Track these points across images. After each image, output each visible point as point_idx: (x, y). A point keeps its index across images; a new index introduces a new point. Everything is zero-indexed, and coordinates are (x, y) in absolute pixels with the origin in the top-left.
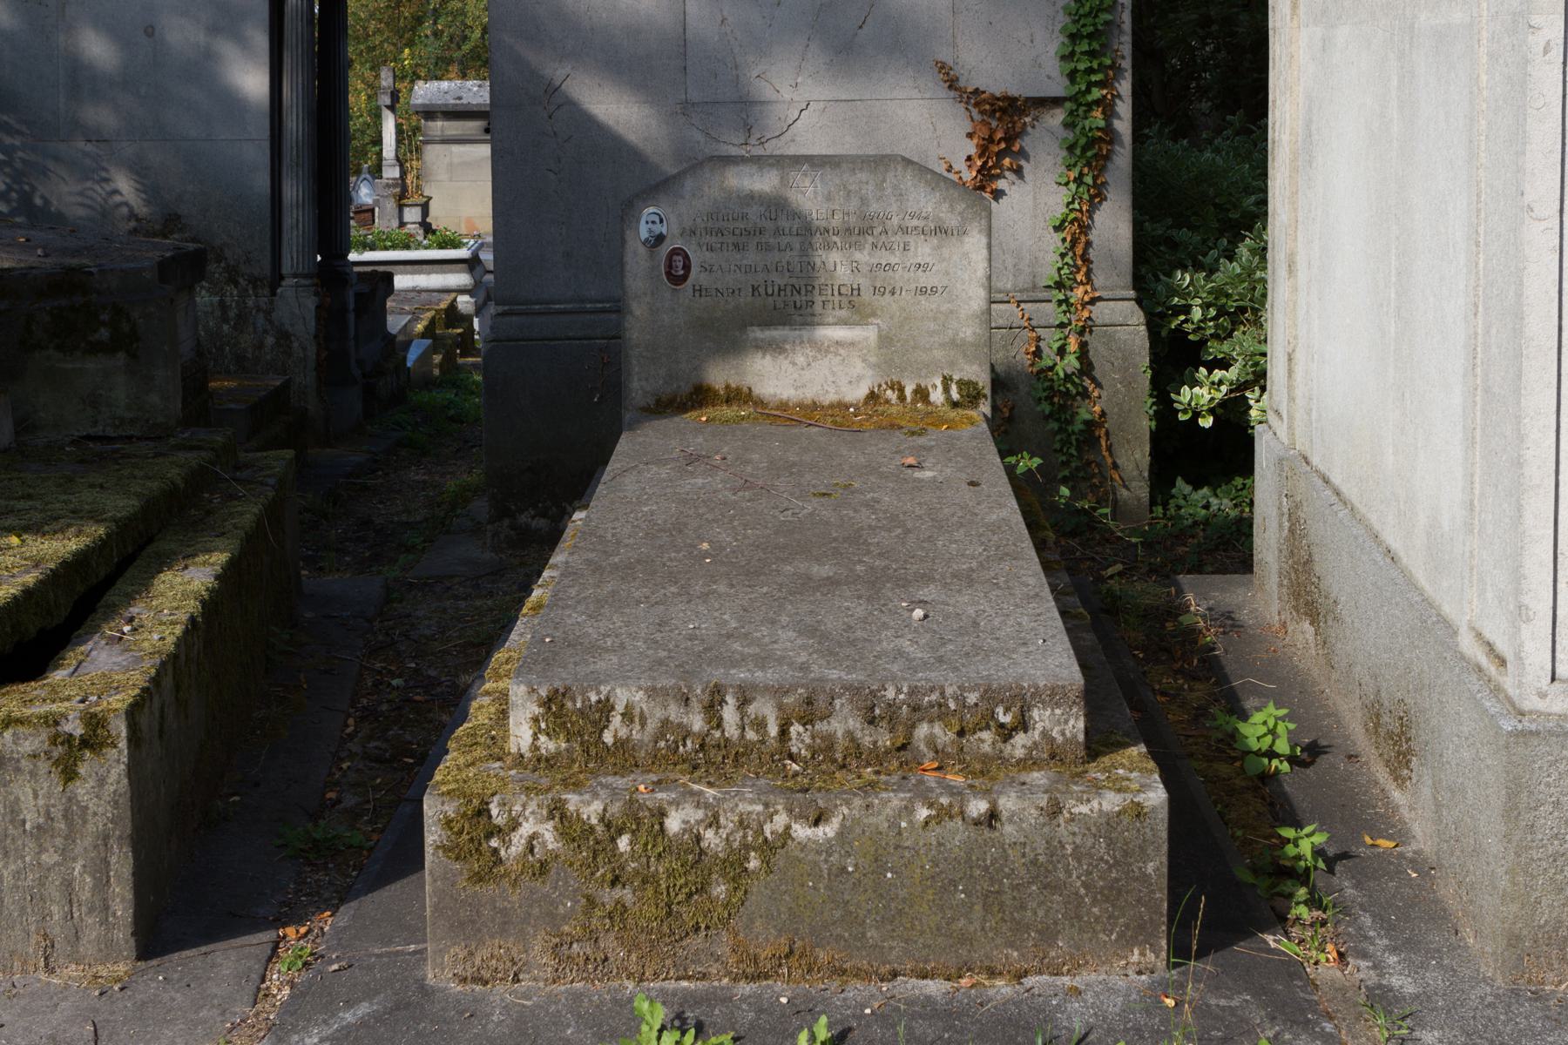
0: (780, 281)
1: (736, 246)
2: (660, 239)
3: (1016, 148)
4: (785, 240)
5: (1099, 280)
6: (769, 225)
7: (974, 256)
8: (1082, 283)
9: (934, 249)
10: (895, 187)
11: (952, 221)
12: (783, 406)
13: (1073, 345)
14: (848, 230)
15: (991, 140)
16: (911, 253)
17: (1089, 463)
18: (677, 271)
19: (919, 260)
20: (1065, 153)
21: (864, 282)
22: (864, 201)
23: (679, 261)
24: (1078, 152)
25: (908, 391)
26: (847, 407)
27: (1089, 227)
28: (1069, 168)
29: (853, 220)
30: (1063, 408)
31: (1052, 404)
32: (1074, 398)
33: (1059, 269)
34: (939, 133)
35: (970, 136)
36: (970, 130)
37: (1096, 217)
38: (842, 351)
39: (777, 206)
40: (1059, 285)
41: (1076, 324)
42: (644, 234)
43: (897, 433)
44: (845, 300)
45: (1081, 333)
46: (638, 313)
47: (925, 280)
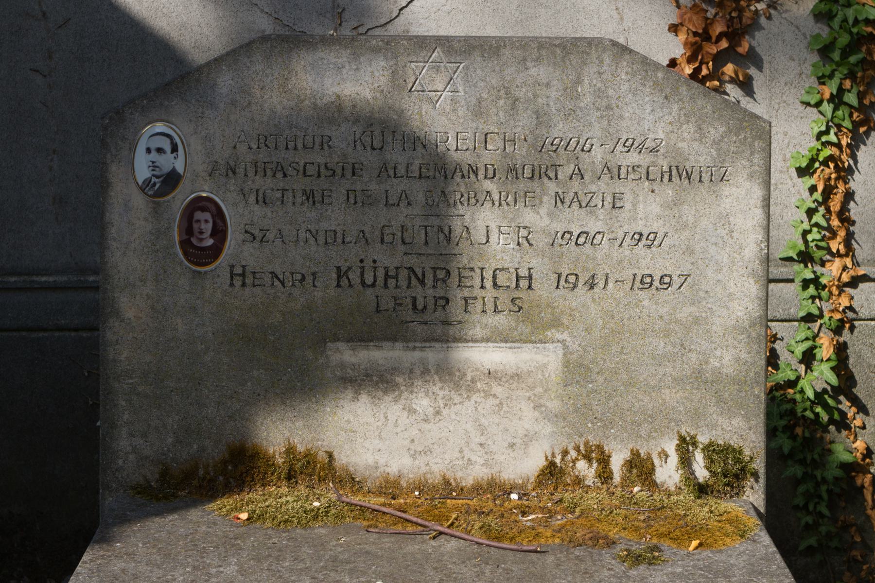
0: (387, 260)
1: (309, 195)
2: (171, 180)
3: (743, 49)
4: (397, 186)
5: (862, 251)
6: (370, 159)
7: (738, 221)
8: (839, 255)
9: (666, 206)
10: (599, 93)
11: (700, 156)
12: (390, 488)
13: (826, 349)
14: (512, 169)
15: (705, 36)
16: (624, 214)
17: (846, 527)
18: (200, 238)
19: (640, 226)
20: (815, 58)
21: (539, 265)
22: (541, 117)
23: (205, 222)
24: (836, 56)
25: (617, 463)
26: (506, 490)
27: (850, 171)
28: (822, 80)
29: (521, 153)
30: (809, 443)
31: (794, 437)
32: (825, 429)
33: (805, 233)
34: (627, 24)
35: (674, 29)
36: (675, 20)
37: (861, 154)
38: (497, 390)
39: (384, 133)
40: (805, 258)
41: (830, 317)
42: (143, 172)
43: (607, 557)
44: (504, 298)
45: (838, 331)
46: (129, 313)
47: (651, 262)
